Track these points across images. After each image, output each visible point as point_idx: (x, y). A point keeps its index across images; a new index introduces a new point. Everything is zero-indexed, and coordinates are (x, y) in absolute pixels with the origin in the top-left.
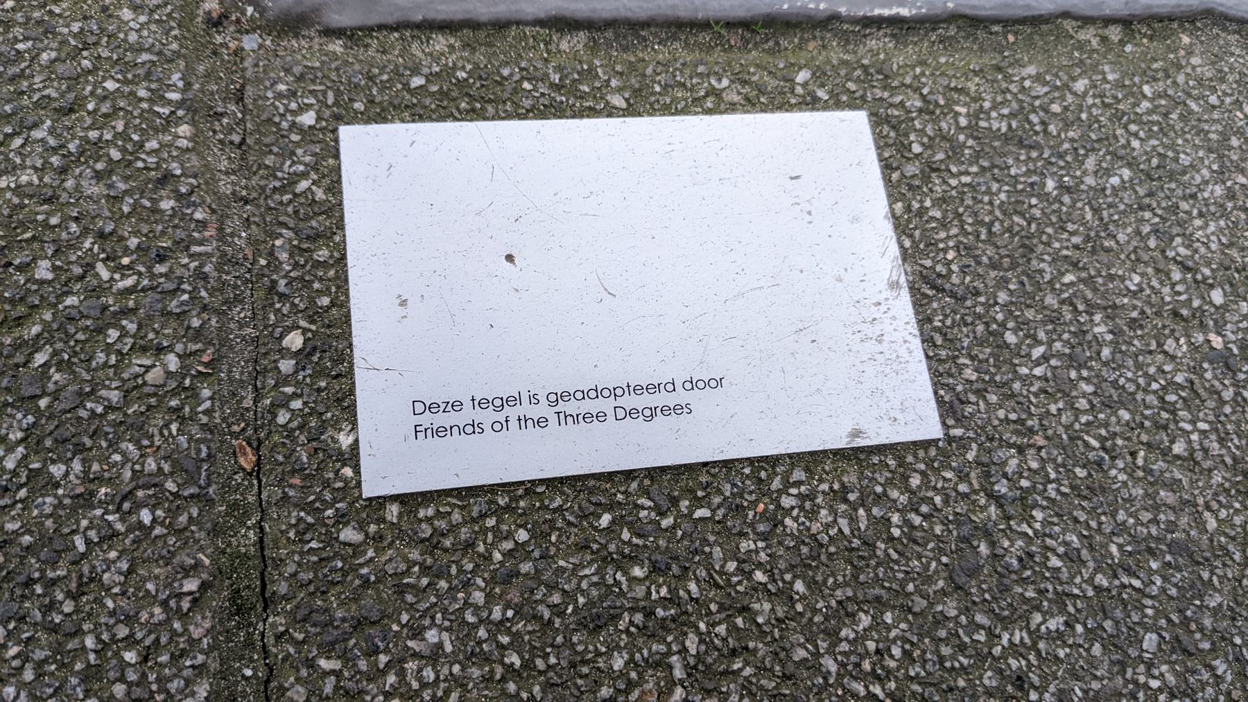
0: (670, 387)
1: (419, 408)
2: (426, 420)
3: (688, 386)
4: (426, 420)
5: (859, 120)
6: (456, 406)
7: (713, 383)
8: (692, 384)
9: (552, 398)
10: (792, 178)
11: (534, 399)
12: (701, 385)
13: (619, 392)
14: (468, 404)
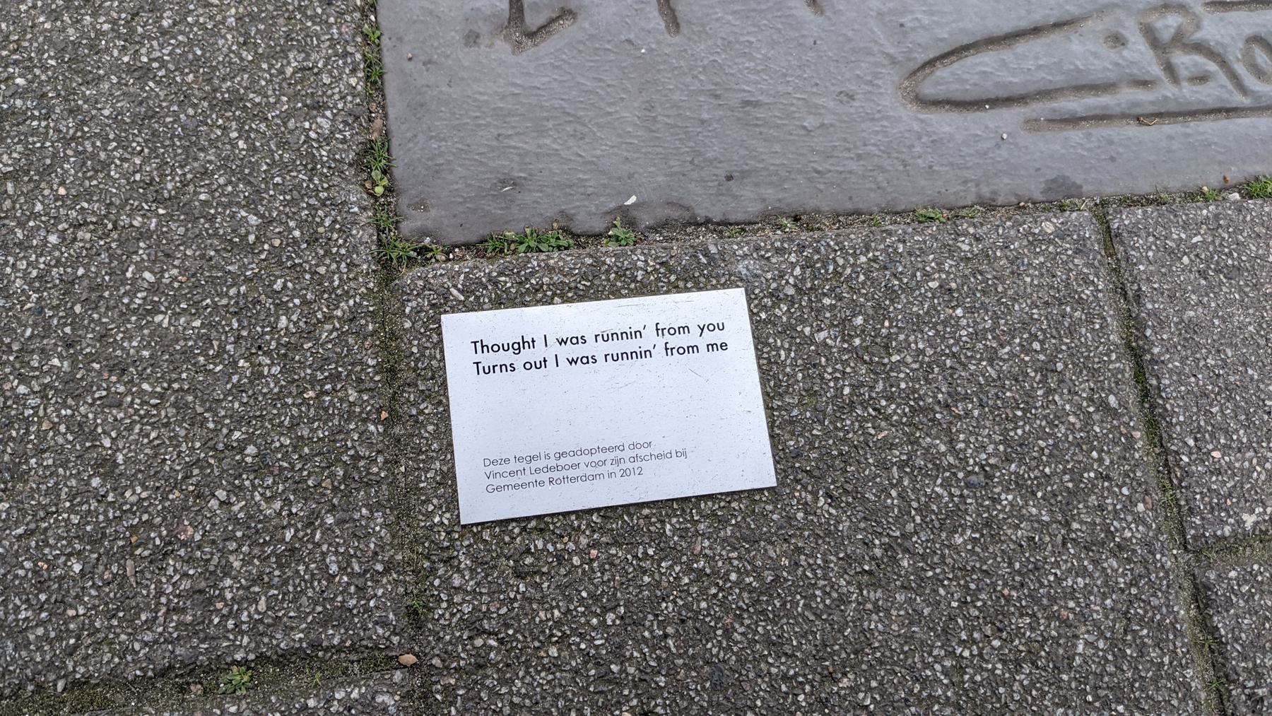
1: (487, 463)
3: (632, 447)
6: (507, 461)
7: (600, 463)
9: (557, 455)
12: (586, 452)
14: (512, 460)
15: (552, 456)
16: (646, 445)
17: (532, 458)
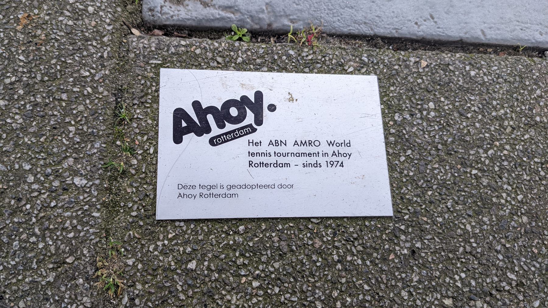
0: (273, 187)
1: (180, 187)
2: (182, 191)
3: (280, 187)
4: (182, 191)
5: (373, 79)
6: (193, 187)
9: (229, 187)
10: (292, 186)
11: (222, 187)
12: (285, 187)
13: (254, 187)
14: (198, 187)
15: (225, 187)
17: (211, 187)
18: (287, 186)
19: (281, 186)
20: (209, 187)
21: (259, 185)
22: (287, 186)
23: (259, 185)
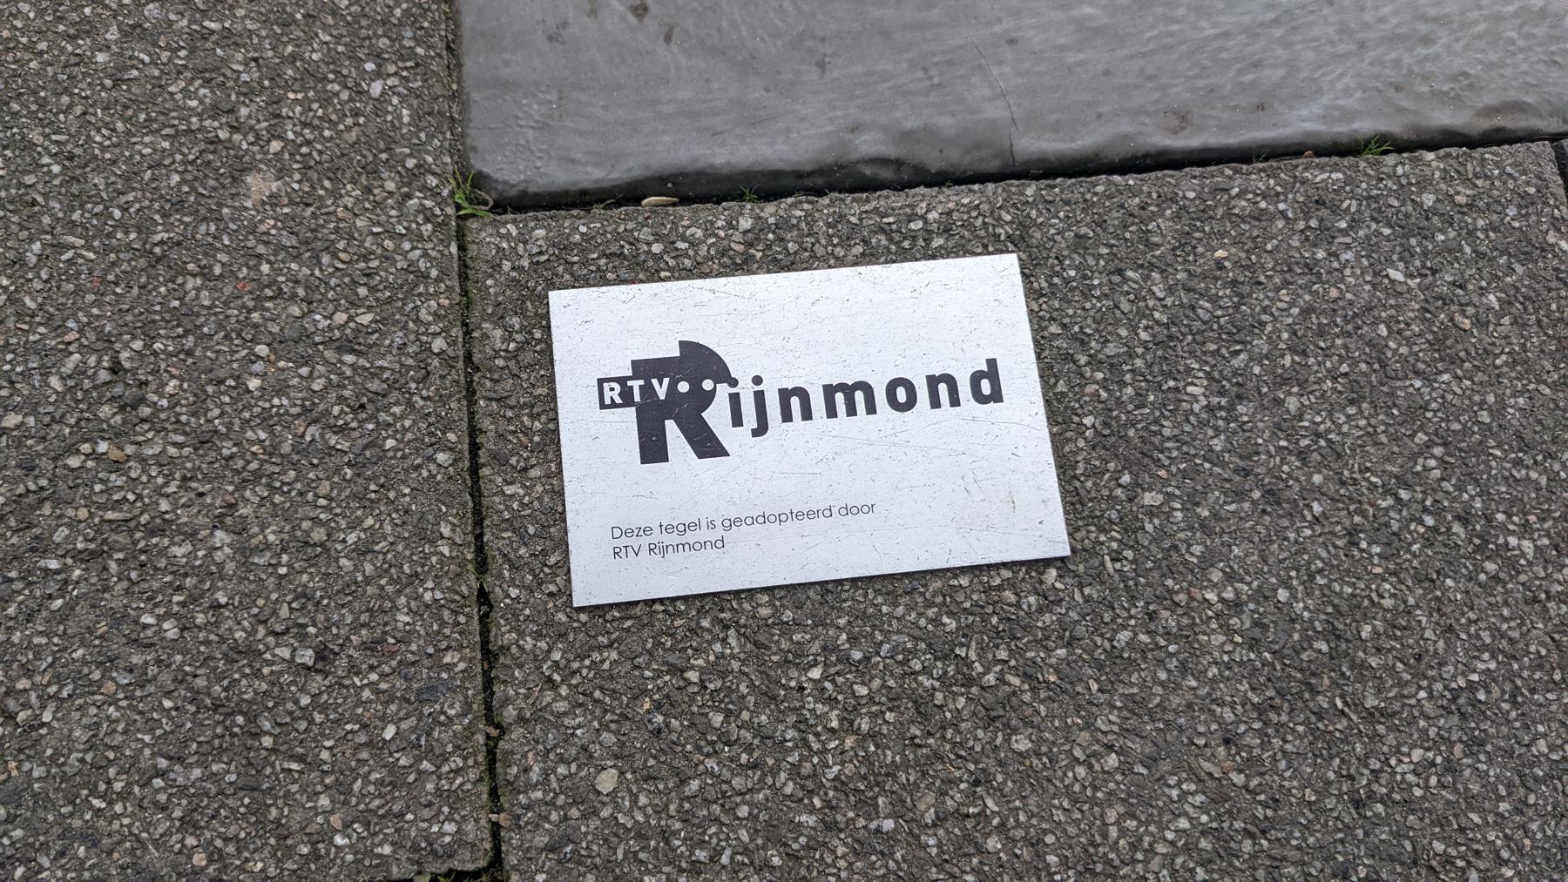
0: (827, 513)
1: (617, 533)
3: (843, 511)
6: (647, 531)
8: (735, 522)
9: (727, 523)
11: (711, 525)
12: (854, 510)
14: (656, 529)
15: (717, 523)
16: (865, 509)
18: (860, 510)
19: (848, 510)
20: (681, 528)
21: (795, 512)
22: (860, 510)
23: (795, 512)
